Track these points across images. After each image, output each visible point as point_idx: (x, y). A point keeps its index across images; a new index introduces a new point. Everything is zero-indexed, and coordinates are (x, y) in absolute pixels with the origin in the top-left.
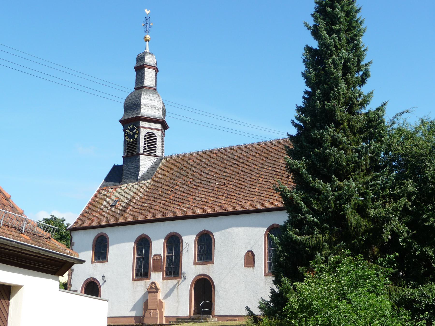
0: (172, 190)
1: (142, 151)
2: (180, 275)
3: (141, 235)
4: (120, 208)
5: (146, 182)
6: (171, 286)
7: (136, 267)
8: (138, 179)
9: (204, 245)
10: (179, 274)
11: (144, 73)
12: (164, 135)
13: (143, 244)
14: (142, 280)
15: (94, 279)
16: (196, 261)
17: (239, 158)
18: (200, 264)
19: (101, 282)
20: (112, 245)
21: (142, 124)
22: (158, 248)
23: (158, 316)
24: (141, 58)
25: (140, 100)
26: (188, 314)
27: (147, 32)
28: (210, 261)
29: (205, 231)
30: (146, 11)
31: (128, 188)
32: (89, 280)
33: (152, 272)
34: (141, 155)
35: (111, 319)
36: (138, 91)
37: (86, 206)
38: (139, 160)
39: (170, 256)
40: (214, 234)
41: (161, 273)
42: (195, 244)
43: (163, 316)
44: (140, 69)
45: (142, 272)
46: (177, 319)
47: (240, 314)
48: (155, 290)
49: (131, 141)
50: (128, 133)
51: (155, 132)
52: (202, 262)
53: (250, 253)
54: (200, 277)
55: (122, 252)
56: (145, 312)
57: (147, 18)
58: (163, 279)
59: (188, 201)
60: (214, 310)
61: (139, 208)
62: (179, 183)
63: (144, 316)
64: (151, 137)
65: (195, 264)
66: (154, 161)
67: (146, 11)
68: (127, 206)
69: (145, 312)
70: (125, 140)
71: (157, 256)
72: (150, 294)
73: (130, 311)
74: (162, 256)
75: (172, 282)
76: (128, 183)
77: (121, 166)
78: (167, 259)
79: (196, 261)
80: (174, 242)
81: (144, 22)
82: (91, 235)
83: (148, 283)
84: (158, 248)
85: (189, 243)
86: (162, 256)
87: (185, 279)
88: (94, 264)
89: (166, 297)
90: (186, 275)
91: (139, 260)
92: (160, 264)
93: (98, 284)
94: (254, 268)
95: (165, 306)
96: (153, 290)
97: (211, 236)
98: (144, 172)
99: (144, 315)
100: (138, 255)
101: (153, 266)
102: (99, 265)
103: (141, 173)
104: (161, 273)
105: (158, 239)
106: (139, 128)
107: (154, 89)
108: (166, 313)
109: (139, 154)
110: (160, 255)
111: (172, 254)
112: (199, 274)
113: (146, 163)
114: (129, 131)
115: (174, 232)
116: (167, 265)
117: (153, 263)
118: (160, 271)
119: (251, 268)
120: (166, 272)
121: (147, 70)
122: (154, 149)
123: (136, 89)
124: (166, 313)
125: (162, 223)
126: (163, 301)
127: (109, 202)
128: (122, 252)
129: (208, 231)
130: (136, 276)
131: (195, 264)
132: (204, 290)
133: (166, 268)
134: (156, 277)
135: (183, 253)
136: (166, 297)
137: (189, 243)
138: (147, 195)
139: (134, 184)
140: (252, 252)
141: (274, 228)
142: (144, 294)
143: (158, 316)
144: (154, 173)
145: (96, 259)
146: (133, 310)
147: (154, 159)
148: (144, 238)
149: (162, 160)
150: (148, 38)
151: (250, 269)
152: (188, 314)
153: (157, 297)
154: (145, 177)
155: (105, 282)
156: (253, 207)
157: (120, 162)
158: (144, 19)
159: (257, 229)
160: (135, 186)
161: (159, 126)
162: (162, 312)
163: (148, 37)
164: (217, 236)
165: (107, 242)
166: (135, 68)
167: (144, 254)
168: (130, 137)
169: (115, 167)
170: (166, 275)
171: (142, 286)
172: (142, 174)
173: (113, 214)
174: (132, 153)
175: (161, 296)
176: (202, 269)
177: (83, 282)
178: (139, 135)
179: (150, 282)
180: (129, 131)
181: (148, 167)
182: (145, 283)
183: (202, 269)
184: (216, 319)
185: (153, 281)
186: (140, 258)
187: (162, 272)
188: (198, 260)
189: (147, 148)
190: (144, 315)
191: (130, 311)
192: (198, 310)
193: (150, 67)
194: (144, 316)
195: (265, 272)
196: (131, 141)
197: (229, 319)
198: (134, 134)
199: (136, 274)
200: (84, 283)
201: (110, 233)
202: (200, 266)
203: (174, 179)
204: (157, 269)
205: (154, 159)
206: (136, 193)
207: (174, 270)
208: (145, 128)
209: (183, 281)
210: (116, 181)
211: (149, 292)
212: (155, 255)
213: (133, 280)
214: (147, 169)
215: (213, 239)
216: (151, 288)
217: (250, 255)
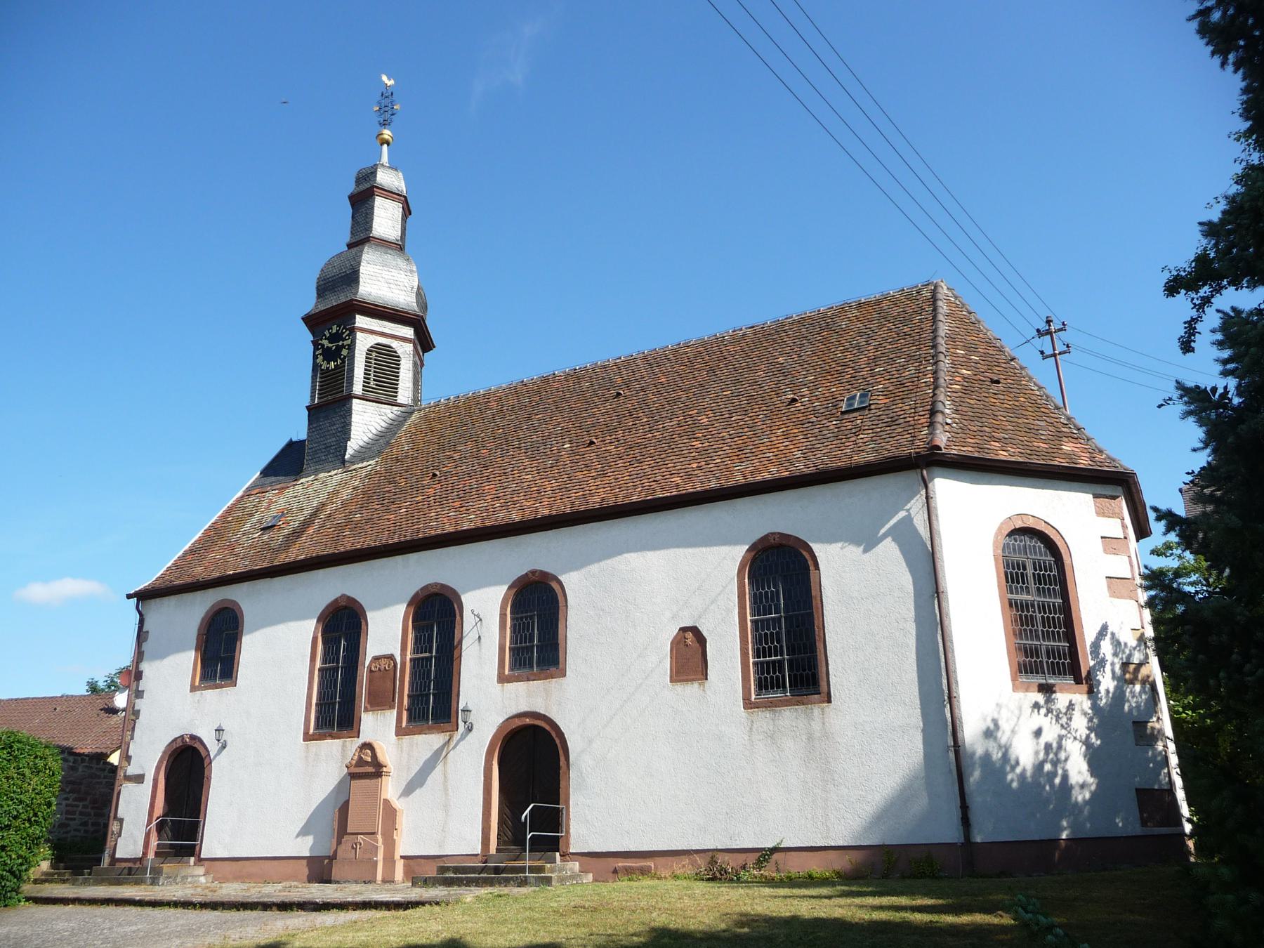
0: (435, 475)
1: (358, 388)
2: (453, 719)
3: (336, 601)
4: (285, 532)
5: (365, 464)
6: (427, 755)
7: (319, 698)
8: (344, 462)
9: (532, 618)
10: (449, 716)
11: (373, 208)
12: (422, 365)
13: (343, 625)
14: (333, 737)
15: (193, 737)
16: (507, 672)
17: (628, 384)
18: (518, 679)
19: (212, 746)
20: (251, 632)
21: (361, 321)
22: (386, 633)
23: (380, 857)
24: (367, 176)
25: (359, 264)
26: (478, 850)
27: (384, 124)
28: (553, 669)
29: (533, 572)
30: (384, 78)
31: (316, 485)
32: (179, 743)
33: (366, 710)
34: (355, 401)
35: (234, 863)
36: (354, 250)
37: (199, 534)
38: (349, 412)
39: (423, 659)
40: (561, 578)
41: (394, 714)
42: (503, 615)
43: (397, 857)
44: (362, 199)
45: (335, 712)
46: (443, 870)
47: (675, 848)
48: (371, 769)
49: (332, 365)
50: (323, 346)
51: (395, 344)
52: (524, 672)
53: (689, 635)
54: (518, 723)
55: (281, 650)
56: (339, 843)
57: (387, 96)
58: (400, 732)
59: (481, 496)
60: (568, 832)
61: (337, 526)
62: (456, 456)
63: (333, 858)
64: (384, 360)
65: (502, 679)
66: (391, 416)
67: (384, 78)
68: (306, 524)
69: (339, 843)
70: (315, 367)
71: (383, 661)
72: (356, 784)
73: (298, 836)
74: (398, 661)
75: (429, 742)
76: (316, 472)
77: (302, 443)
78: (413, 667)
79: (507, 672)
80: (436, 615)
81: (379, 103)
82: (196, 609)
83: (353, 745)
84: (386, 633)
85: (484, 613)
86: (398, 661)
87: (470, 729)
88: (198, 693)
89: (408, 790)
90: (472, 718)
91: (327, 676)
92: (389, 684)
93: (203, 753)
94: (707, 683)
95: (405, 823)
96: (368, 768)
97: (554, 585)
98: (361, 443)
99: (335, 852)
100: (324, 661)
101: (370, 693)
102: (213, 697)
103: (352, 446)
104: (394, 714)
105: (383, 604)
106: (353, 331)
107: (399, 247)
108: (406, 844)
109: (350, 397)
110: (391, 657)
111: (431, 652)
112: (514, 711)
113: (367, 420)
114: (325, 342)
115: (436, 584)
116: (411, 689)
117: (370, 681)
118: (392, 707)
119: (696, 684)
120: (409, 710)
121: (379, 201)
122: (395, 387)
123: (350, 246)
124: (406, 844)
125: (399, 559)
126: (397, 804)
127: (259, 521)
128: (281, 650)
129: (545, 575)
130: (317, 726)
131: (502, 679)
132: (532, 766)
133: (409, 696)
134: (378, 727)
135: (464, 647)
136: (408, 790)
137: (484, 613)
138: (364, 493)
139: (333, 473)
140: (695, 631)
141: (772, 547)
142: (340, 783)
143: (380, 857)
144: (388, 443)
145: (204, 677)
146: (304, 832)
147: (390, 412)
148: (346, 608)
149: (412, 413)
150: (386, 137)
151: (692, 689)
152: (478, 850)
153: (377, 791)
154: (362, 455)
155: (224, 747)
156: (692, 487)
157: (300, 432)
158: (379, 98)
159: (725, 550)
160: (334, 477)
161: (408, 332)
162: (394, 842)
163: (387, 134)
164: (580, 588)
165: (237, 627)
166: (351, 198)
167: (344, 657)
168: (329, 355)
169: (291, 444)
170: (410, 719)
171: (335, 755)
172: (356, 447)
173: (266, 547)
174: (330, 404)
175: (390, 788)
176: (526, 697)
177: (162, 748)
178: (352, 348)
179: (359, 742)
180: (325, 342)
181: (374, 431)
182: (344, 746)
183: (526, 697)
184: (576, 866)
185: (368, 740)
186: (329, 669)
187: (395, 712)
188: (511, 669)
189: (372, 384)
190: (335, 852)
191: (298, 836)
192: (512, 834)
193: (390, 194)
194: (333, 858)
195: (746, 699)
196: (332, 365)
197: (621, 863)
198: (340, 348)
199: (317, 719)
200: (164, 752)
201: (245, 597)
202: (519, 688)
203: (442, 448)
204: (379, 701)
205: (390, 412)
206: (334, 494)
207: (433, 702)
208: (368, 335)
209: (462, 738)
210: (287, 474)
211: (353, 776)
212: (376, 659)
213: (307, 737)
214: (370, 436)
215: (560, 598)
216: (361, 762)
217: (689, 642)
